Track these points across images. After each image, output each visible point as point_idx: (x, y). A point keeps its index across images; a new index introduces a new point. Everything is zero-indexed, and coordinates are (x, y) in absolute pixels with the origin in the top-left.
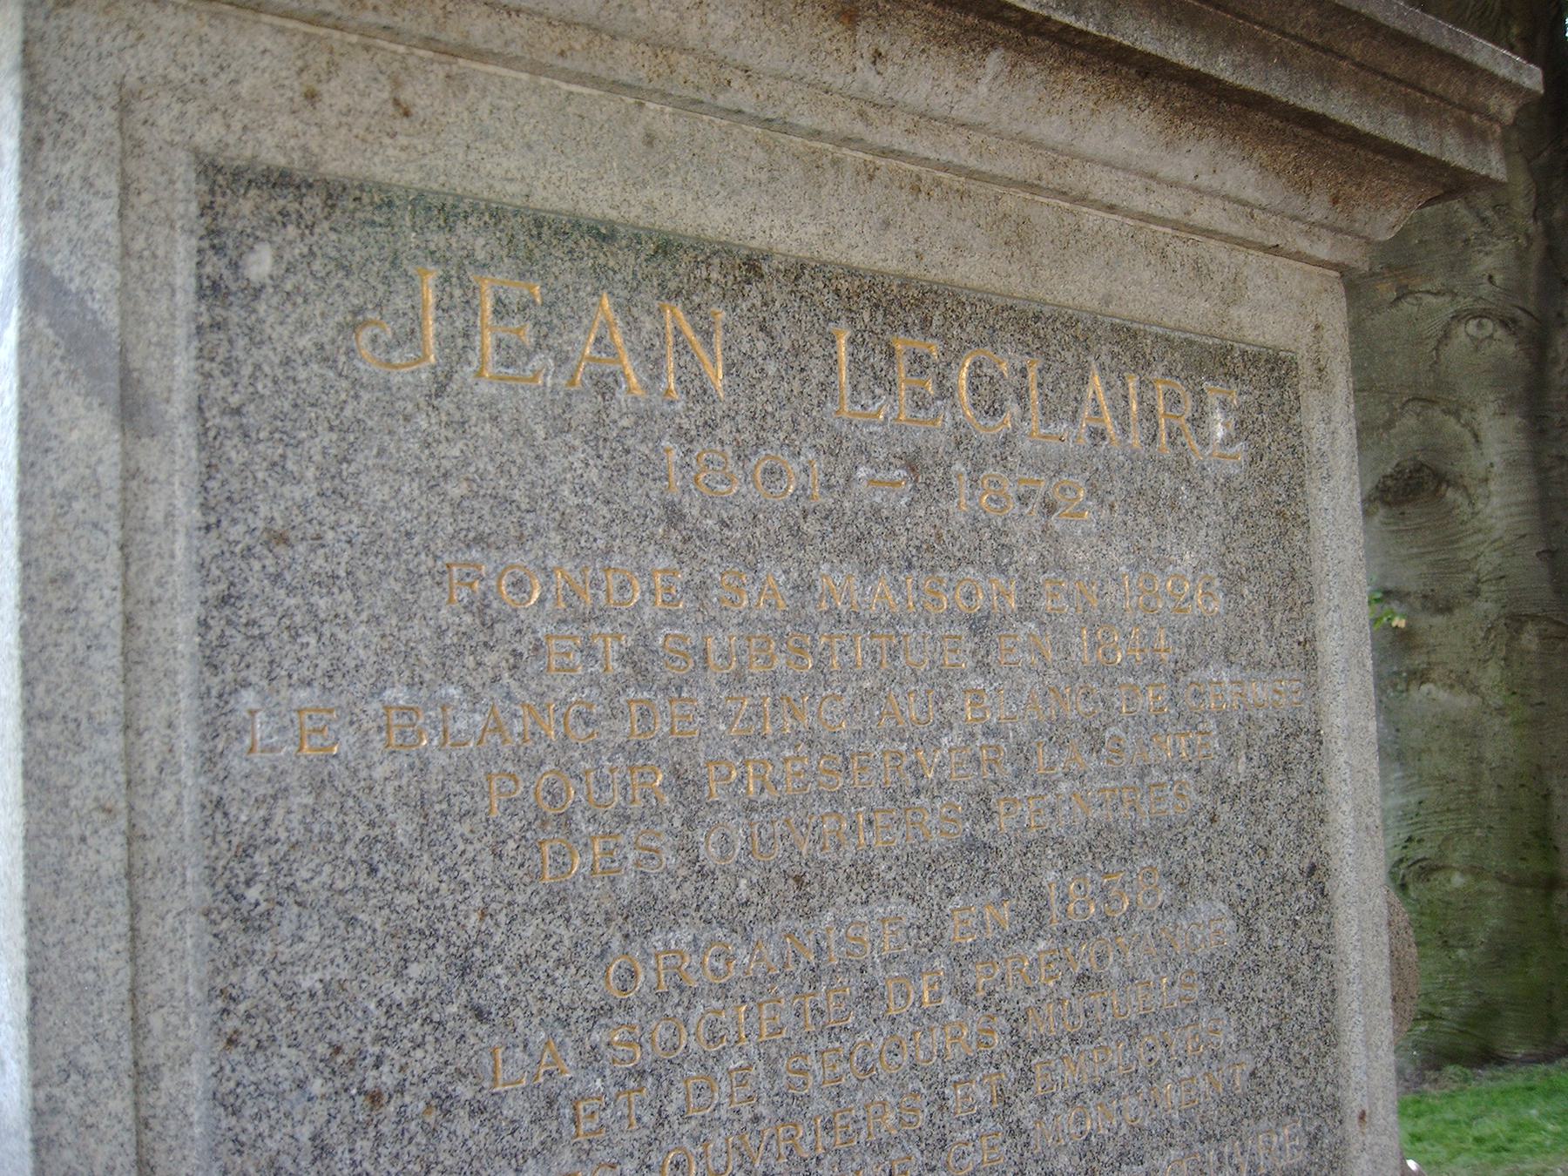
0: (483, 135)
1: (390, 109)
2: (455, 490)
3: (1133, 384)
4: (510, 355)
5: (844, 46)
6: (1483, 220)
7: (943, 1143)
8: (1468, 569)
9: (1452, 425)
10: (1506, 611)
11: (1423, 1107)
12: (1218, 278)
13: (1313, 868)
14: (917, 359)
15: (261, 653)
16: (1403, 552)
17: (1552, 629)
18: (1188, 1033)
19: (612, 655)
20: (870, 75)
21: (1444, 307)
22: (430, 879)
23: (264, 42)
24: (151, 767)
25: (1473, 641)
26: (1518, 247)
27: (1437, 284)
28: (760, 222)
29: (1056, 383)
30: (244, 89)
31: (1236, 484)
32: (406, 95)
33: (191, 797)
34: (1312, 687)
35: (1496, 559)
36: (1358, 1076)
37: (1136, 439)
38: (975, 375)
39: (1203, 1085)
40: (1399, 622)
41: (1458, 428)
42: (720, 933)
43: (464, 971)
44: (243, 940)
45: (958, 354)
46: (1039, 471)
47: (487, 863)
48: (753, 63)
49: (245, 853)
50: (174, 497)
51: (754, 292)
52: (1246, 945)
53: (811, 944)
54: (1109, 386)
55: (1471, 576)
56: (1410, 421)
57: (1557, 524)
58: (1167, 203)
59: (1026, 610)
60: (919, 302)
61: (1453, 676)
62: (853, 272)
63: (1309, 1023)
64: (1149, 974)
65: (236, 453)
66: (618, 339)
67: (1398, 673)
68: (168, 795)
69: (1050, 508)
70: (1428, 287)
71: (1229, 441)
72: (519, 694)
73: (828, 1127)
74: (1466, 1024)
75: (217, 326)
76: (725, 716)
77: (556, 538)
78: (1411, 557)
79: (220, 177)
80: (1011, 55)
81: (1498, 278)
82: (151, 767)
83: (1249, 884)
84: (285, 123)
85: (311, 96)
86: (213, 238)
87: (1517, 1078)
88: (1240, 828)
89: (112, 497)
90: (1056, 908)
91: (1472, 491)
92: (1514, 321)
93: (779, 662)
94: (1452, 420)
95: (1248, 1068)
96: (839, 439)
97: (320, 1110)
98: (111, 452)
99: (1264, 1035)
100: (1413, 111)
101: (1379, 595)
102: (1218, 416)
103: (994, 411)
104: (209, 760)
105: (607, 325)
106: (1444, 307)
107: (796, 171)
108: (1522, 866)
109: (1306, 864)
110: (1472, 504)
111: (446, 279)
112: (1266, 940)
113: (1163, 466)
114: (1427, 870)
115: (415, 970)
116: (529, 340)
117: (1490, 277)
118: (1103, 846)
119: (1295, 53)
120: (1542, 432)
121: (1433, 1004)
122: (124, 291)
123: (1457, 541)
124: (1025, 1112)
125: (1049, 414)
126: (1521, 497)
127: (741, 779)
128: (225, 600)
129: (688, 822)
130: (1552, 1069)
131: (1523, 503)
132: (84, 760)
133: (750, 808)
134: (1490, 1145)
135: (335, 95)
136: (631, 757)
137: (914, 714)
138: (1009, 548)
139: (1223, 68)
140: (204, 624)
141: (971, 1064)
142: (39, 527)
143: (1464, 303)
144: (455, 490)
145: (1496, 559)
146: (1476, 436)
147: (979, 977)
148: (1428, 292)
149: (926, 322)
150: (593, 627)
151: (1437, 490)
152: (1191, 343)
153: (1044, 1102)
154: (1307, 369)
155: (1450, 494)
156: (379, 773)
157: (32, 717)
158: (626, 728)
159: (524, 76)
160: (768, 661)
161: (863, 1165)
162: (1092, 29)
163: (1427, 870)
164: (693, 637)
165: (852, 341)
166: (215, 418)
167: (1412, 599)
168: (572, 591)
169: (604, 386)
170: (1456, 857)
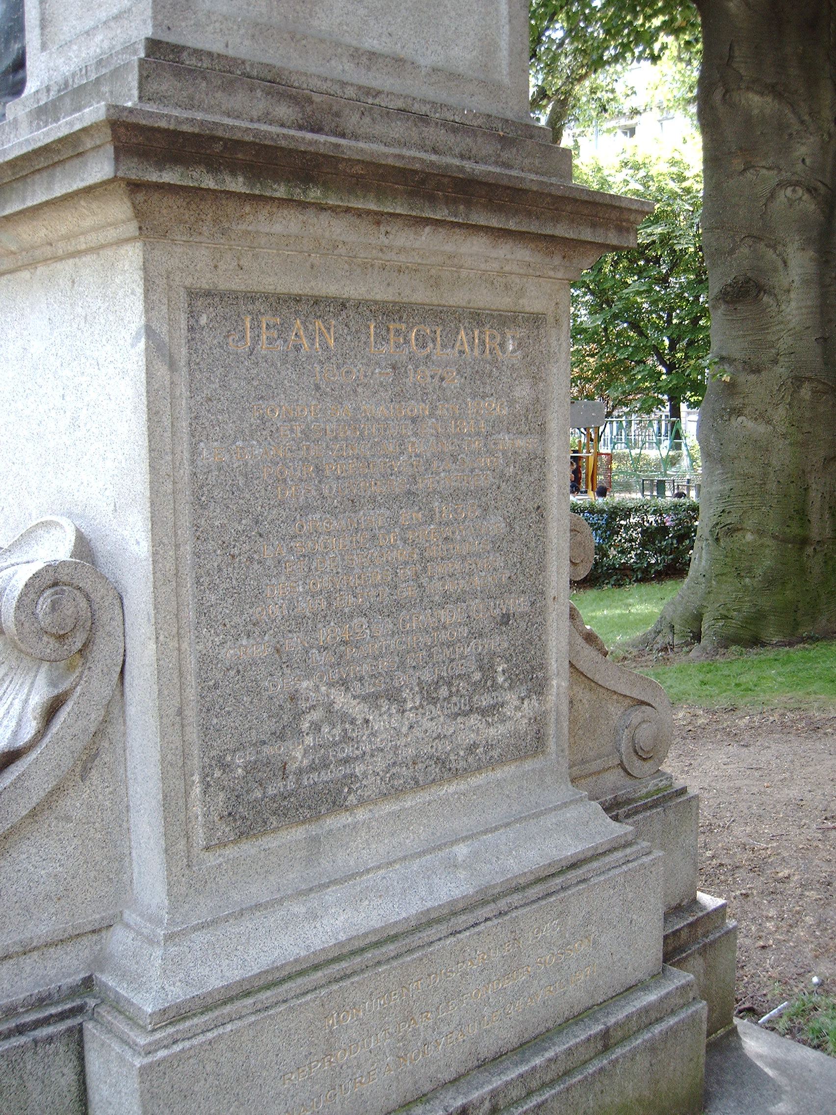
0: (263, 272)
1: (237, 268)
2: (255, 383)
3: (476, 333)
4: (270, 341)
5: (376, 232)
6: (802, 122)
7: (396, 587)
8: (773, 347)
9: (770, 254)
10: (793, 374)
11: (712, 668)
12: (515, 289)
13: (539, 507)
14: (397, 331)
15: (205, 432)
16: (734, 333)
17: (820, 387)
18: (485, 561)
19: (299, 431)
20: (384, 239)
21: (772, 177)
22: (248, 496)
23: (203, 252)
24: (178, 464)
25: (771, 391)
26: (823, 141)
27: (770, 162)
28: (346, 289)
29: (447, 335)
30: (198, 268)
31: (516, 367)
32: (241, 263)
33: (187, 472)
34: (543, 441)
35: (790, 341)
36: (554, 584)
37: (476, 352)
38: (417, 335)
39: (490, 579)
40: (726, 378)
41: (774, 256)
42: (328, 516)
43: (257, 523)
44: (201, 511)
45: (412, 328)
46: (439, 366)
47: (263, 493)
48: (346, 240)
49: (201, 487)
50: (182, 390)
51: (344, 313)
52: (509, 533)
53: (356, 521)
54: (467, 334)
55: (773, 351)
56: (745, 250)
57: (830, 321)
58: (494, 265)
59: (432, 415)
60: (399, 311)
61: (757, 413)
62: (376, 302)
63: (533, 563)
64: (471, 539)
65: (198, 376)
66: (302, 333)
67: (725, 409)
68: (182, 471)
69: (442, 379)
70: (763, 163)
71: (514, 351)
72: (272, 443)
73: (360, 578)
74: (747, 623)
75: (193, 339)
76: (332, 450)
77: (283, 396)
78: (738, 337)
79: (193, 294)
80: (434, 227)
81: (808, 161)
82: (178, 464)
83: (512, 511)
84: (208, 275)
85: (216, 267)
86: (192, 314)
87: (770, 653)
88: (509, 491)
89: (168, 390)
90: (438, 515)
91: (779, 297)
92: (816, 190)
93: (348, 433)
94: (771, 251)
95: (508, 575)
96: (370, 360)
97: (220, 558)
98: (168, 378)
99: (515, 565)
100: (594, 226)
101: (717, 360)
102: (511, 342)
103: (424, 347)
104: (193, 462)
105: (299, 329)
106: (772, 177)
107: (359, 270)
108: (788, 530)
109: (536, 506)
110: (778, 305)
111: (253, 319)
112: (517, 531)
113: (487, 362)
114: (732, 530)
115: (244, 522)
116: (276, 336)
117: (803, 160)
118: (456, 495)
119: (542, 213)
120: (827, 262)
121: (728, 610)
122: (169, 331)
123: (767, 329)
124: (424, 580)
125: (444, 346)
126: (809, 303)
127: (336, 469)
128: (196, 418)
129: (320, 482)
130: (792, 650)
131: (809, 307)
132: (163, 462)
133: (338, 478)
134: (742, 687)
135: (222, 266)
136: (303, 462)
137: (391, 449)
138: (427, 394)
139: (512, 225)
140: (191, 424)
141: (406, 563)
142: (152, 399)
143: (786, 175)
144: (255, 383)
145: (790, 341)
146: (785, 262)
147: (410, 535)
148: (763, 167)
149: (401, 318)
150: (293, 423)
151: (757, 296)
152: (501, 315)
153: (431, 578)
154: (550, 319)
155: (766, 299)
156: (235, 466)
157: (151, 450)
158: (303, 453)
159: (275, 251)
160: (345, 433)
161: (370, 591)
162: (461, 221)
163: (732, 530)
164: (322, 426)
165: (375, 327)
166: (193, 366)
167: (736, 363)
168: (287, 412)
169: (297, 348)
170: (749, 524)
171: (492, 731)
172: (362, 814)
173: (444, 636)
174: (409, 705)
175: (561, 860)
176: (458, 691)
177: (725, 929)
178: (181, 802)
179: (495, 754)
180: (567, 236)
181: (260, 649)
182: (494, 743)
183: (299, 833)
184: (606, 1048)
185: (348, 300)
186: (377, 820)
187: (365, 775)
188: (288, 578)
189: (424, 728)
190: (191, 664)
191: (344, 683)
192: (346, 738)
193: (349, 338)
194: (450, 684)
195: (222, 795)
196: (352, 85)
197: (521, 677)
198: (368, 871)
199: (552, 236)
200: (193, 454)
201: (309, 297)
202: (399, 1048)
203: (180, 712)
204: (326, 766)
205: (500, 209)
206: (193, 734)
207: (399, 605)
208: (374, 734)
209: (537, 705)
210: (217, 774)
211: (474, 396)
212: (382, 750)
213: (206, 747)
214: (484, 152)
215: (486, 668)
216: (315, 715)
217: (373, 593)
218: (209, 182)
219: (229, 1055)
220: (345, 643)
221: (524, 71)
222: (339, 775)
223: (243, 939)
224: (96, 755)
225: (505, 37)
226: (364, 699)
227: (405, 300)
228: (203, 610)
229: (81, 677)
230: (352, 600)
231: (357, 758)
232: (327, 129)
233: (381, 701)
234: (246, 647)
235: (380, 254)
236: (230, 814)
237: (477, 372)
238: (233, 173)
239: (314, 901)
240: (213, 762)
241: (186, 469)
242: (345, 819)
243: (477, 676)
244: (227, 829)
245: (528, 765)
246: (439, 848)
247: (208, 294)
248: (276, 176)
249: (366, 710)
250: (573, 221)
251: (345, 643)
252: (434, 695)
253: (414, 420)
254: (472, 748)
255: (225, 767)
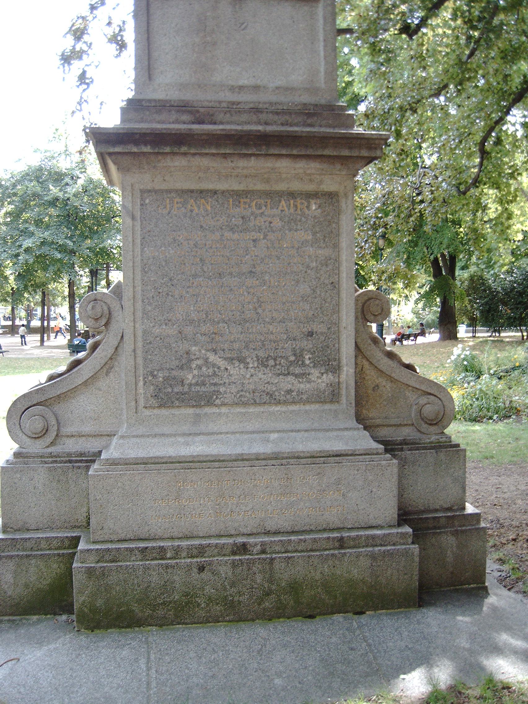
2: (171, 225)
3: (292, 202)
36: (344, 321)
37: (292, 210)
49: (145, 265)
50: (138, 228)
51: (216, 196)
54: (286, 203)
59: (264, 238)
64: (288, 295)
65: (144, 222)
69: (271, 223)
71: (316, 209)
79: (142, 191)
84: (150, 184)
85: (153, 181)
86: (142, 199)
97: (153, 293)
98: (131, 223)
104: (141, 255)
113: (298, 214)
124: (260, 311)
129: (203, 265)
135: (156, 180)
138: (262, 229)
141: (249, 302)
144: (171, 225)
147: (252, 290)
149: (247, 197)
153: (264, 310)
158: (193, 253)
169: (192, 211)
171: (302, 386)
172: (224, 410)
173: (272, 337)
174: (251, 365)
175: (328, 451)
176: (280, 363)
177: (477, 527)
178: (134, 386)
179: (304, 397)
180: (332, 154)
181: (172, 331)
182: (303, 391)
183: (191, 411)
184: (341, 547)
185: (218, 191)
186: (232, 414)
187: (225, 392)
188: (186, 303)
189: (259, 377)
190: (140, 333)
191: (215, 351)
192: (215, 374)
193: (218, 206)
194: (275, 360)
195: (152, 387)
196: (225, 102)
197: (322, 362)
198: (221, 433)
199: (322, 155)
200: (142, 252)
201: (197, 191)
202: (217, 508)
203: (134, 351)
204: (205, 385)
205: (287, 146)
206: (140, 361)
207: (246, 321)
208: (231, 375)
209: (332, 378)
210: (150, 378)
211: (290, 230)
212: (235, 383)
213: (145, 367)
214: (296, 121)
215: (299, 356)
216: (199, 362)
217: (230, 313)
218: (135, 149)
219: (129, 482)
220: (216, 334)
221: (334, 80)
222: (211, 390)
223: (152, 445)
224: (112, 367)
225: (323, 66)
226: (225, 359)
227: (251, 189)
228: (145, 313)
229: (105, 336)
230: (219, 316)
231: (221, 384)
232: (206, 122)
233: (234, 361)
234: (165, 329)
235: (233, 171)
236: (156, 396)
237: (292, 219)
238: (146, 145)
239: (190, 439)
240: (148, 373)
241: (138, 259)
242: (215, 410)
243: (292, 358)
244: (154, 402)
245: (327, 407)
246: (263, 432)
247: (149, 191)
248: (166, 145)
249: (226, 364)
250: (336, 147)
251: (216, 334)
252: (266, 363)
253: (254, 241)
254: (289, 392)
255: (154, 376)
